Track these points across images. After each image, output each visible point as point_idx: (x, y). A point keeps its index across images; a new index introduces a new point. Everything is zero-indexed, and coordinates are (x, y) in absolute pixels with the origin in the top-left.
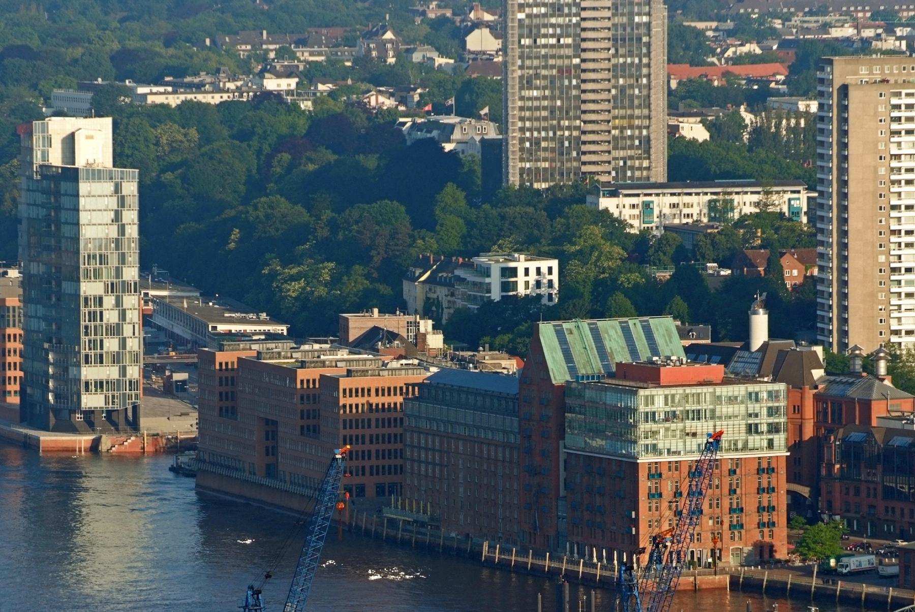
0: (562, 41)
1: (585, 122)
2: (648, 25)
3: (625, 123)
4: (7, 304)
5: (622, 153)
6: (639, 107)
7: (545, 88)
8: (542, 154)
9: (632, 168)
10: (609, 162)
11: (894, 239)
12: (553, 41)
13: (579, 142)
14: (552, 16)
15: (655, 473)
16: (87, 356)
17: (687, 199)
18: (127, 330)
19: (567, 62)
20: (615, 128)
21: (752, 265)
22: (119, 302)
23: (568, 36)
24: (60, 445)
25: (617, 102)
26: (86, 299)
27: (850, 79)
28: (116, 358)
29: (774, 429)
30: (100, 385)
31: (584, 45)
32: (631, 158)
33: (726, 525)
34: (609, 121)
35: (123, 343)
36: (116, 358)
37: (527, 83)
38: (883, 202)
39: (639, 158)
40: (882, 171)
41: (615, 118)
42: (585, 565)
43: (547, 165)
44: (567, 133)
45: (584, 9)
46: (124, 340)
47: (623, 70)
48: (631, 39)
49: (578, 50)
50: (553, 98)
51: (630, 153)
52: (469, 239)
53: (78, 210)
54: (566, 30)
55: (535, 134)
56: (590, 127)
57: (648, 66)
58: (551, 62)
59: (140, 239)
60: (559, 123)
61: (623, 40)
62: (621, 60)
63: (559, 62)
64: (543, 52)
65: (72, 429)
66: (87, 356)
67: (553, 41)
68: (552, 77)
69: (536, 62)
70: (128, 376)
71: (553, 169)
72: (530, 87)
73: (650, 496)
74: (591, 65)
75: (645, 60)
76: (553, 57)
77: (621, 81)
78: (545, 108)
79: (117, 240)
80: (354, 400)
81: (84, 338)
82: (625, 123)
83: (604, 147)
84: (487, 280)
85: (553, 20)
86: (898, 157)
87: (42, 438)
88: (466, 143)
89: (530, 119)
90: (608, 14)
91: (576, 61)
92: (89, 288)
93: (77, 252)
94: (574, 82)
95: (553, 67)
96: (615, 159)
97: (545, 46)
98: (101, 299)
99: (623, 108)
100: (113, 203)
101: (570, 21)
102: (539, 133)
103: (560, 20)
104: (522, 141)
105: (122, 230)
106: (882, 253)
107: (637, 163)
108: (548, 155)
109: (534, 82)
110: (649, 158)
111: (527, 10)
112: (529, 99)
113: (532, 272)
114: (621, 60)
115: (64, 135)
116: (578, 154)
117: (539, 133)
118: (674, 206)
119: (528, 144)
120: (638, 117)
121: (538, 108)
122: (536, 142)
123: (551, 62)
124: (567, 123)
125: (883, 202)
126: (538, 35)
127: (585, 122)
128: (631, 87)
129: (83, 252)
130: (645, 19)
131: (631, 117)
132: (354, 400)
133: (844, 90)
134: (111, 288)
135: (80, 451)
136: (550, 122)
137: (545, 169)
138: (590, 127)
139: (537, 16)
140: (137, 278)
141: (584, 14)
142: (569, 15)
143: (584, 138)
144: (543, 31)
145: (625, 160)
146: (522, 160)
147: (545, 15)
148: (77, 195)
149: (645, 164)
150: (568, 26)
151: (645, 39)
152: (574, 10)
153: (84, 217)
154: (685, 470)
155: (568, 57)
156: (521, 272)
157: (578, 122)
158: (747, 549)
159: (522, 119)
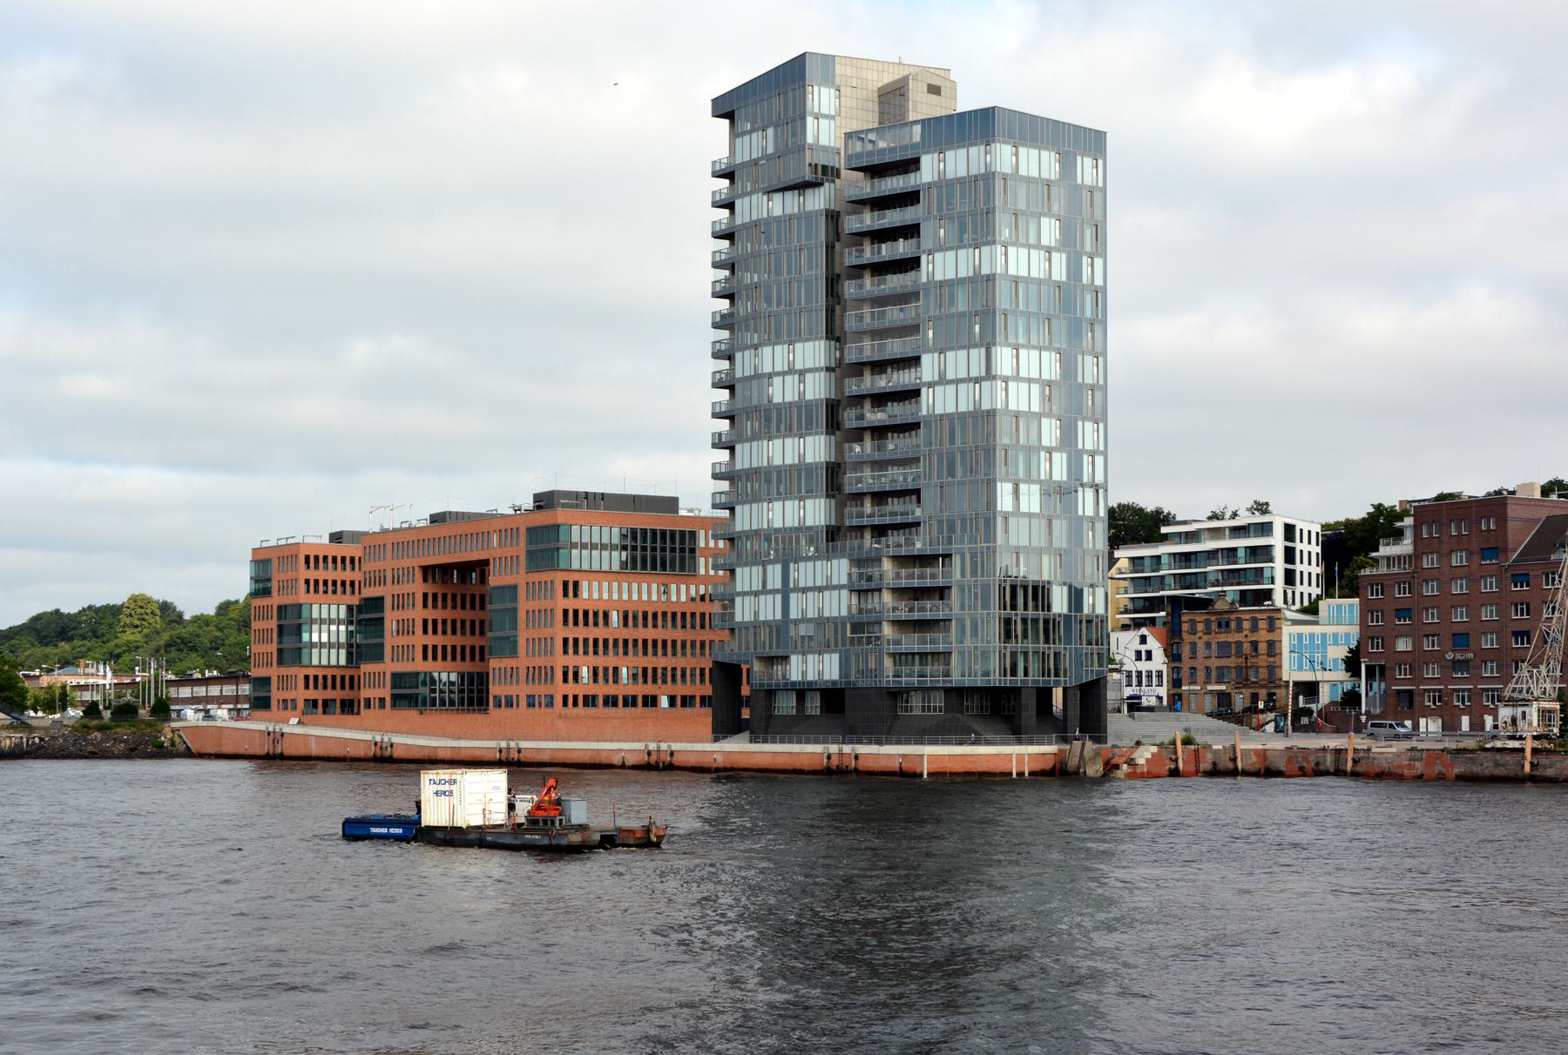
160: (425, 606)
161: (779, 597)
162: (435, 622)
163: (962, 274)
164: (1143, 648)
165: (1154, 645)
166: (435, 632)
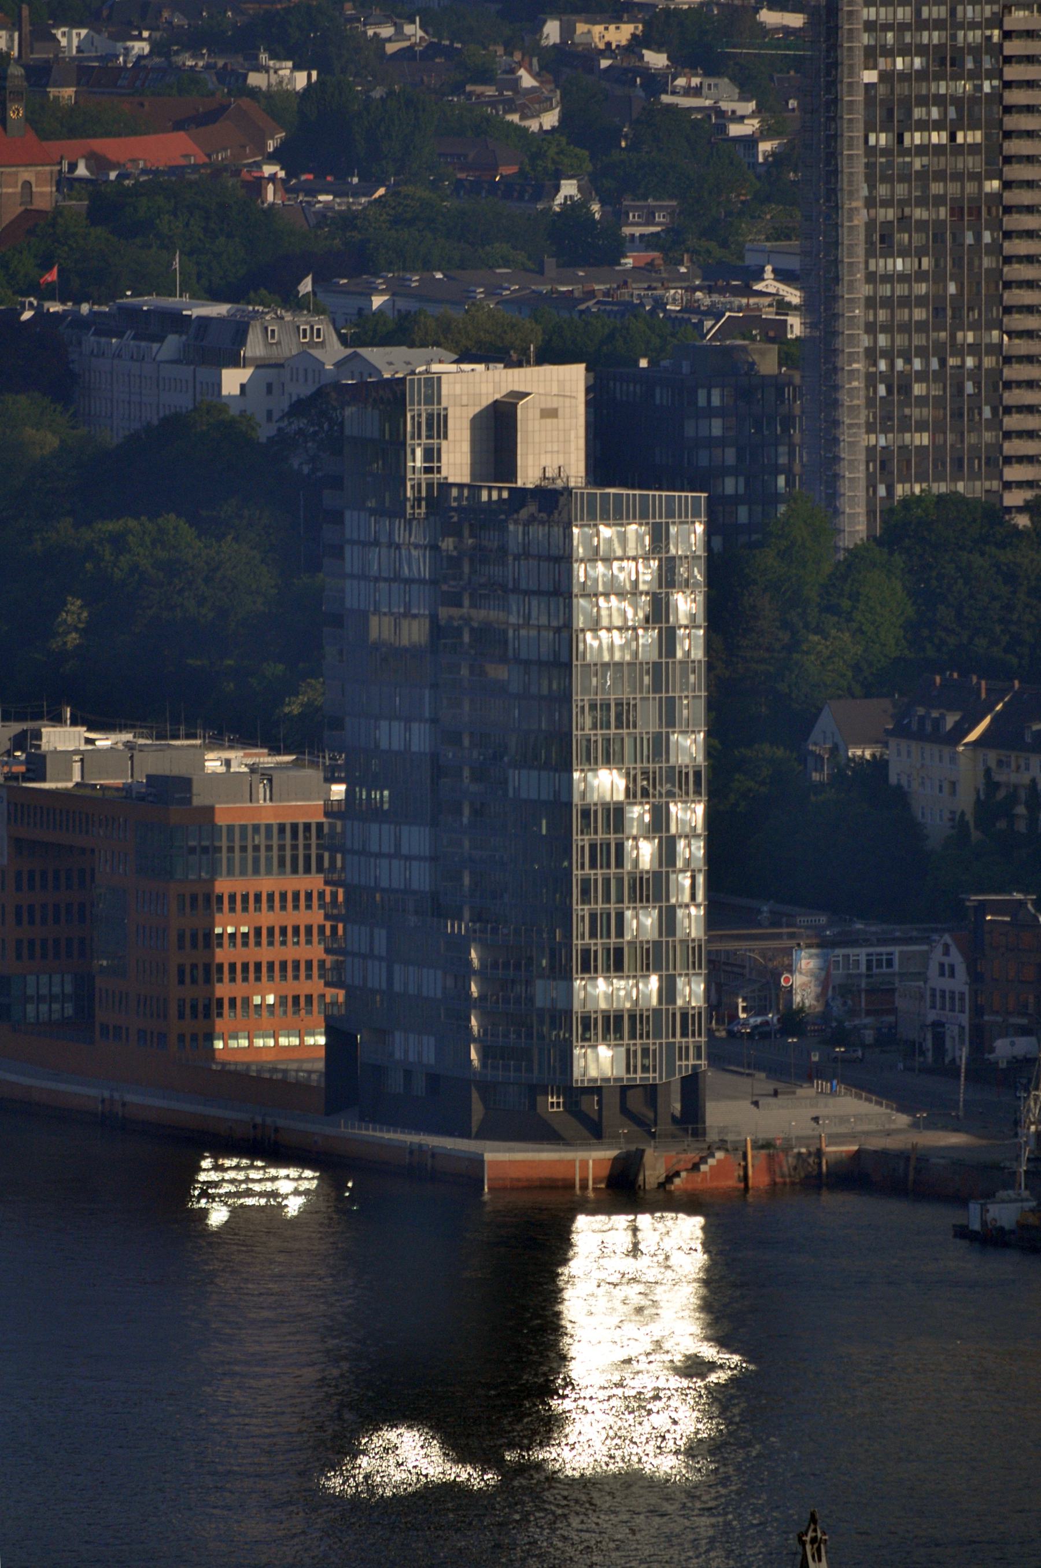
0: (960, 138)
14: (939, 77)
16: (586, 952)
19: (970, 187)
22: (659, 821)
23: (973, 127)
24: (514, 1173)
26: (586, 813)
31: (1013, 147)
35: (668, 920)
37: (882, 241)
43: (923, 439)
44: (970, 362)
45: (1008, 60)
46: (671, 911)
49: (997, 160)
50: (939, 277)
52: (925, 633)
53: (570, 596)
54: (967, 113)
55: (899, 364)
56: (1022, 346)
58: (936, 188)
59: (710, 666)
60: (953, 337)
63: (953, 189)
64: (917, 164)
65: (545, 1133)
68: (940, 224)
69: (901, 190)
71: (939, 449)
72: (888, 252)
74: (1025, 197)
76: (940, 176)
78: (921, 301)
79: (657, 666)
81: (580, 910)
87: (488, 1157)
88: (281, 366)
89: (887, 329)
93: (566, 698)
94: (987, 237)
95: (940, 200)
97: (922, 150)
101: (979, 88)
102: (908, 361)
103: (964, 87)
104: (871, 380)
105: (668, 640)
109: (897, 236)
111: (883, 63)
112: (888, 278)
115: (478, 409)
116: (994, 411)
117: (908, 361)
119: (882, 390)
121: (905, 302)
122: (901, 386)
123: (936, 188)
124: (970, 337)
127: (1010, 334)
135: (584, 1187)
136: (933, 335)
137: (921, 448)
138: (1022, 346)
139: (905, 76)
141: (1012, 73)
142: (975, 75)
143: (1010, 373)
146: (870, 429)
147: (922, 75)
150: (974, 100)
157: (995, 333)
159: (871, 328)
160: (19, 888)
161: (384, 964)
162: (31, 942)
163: (544, 797)
164: (946, 960)
165: (956, 958)
166: (32, 922)
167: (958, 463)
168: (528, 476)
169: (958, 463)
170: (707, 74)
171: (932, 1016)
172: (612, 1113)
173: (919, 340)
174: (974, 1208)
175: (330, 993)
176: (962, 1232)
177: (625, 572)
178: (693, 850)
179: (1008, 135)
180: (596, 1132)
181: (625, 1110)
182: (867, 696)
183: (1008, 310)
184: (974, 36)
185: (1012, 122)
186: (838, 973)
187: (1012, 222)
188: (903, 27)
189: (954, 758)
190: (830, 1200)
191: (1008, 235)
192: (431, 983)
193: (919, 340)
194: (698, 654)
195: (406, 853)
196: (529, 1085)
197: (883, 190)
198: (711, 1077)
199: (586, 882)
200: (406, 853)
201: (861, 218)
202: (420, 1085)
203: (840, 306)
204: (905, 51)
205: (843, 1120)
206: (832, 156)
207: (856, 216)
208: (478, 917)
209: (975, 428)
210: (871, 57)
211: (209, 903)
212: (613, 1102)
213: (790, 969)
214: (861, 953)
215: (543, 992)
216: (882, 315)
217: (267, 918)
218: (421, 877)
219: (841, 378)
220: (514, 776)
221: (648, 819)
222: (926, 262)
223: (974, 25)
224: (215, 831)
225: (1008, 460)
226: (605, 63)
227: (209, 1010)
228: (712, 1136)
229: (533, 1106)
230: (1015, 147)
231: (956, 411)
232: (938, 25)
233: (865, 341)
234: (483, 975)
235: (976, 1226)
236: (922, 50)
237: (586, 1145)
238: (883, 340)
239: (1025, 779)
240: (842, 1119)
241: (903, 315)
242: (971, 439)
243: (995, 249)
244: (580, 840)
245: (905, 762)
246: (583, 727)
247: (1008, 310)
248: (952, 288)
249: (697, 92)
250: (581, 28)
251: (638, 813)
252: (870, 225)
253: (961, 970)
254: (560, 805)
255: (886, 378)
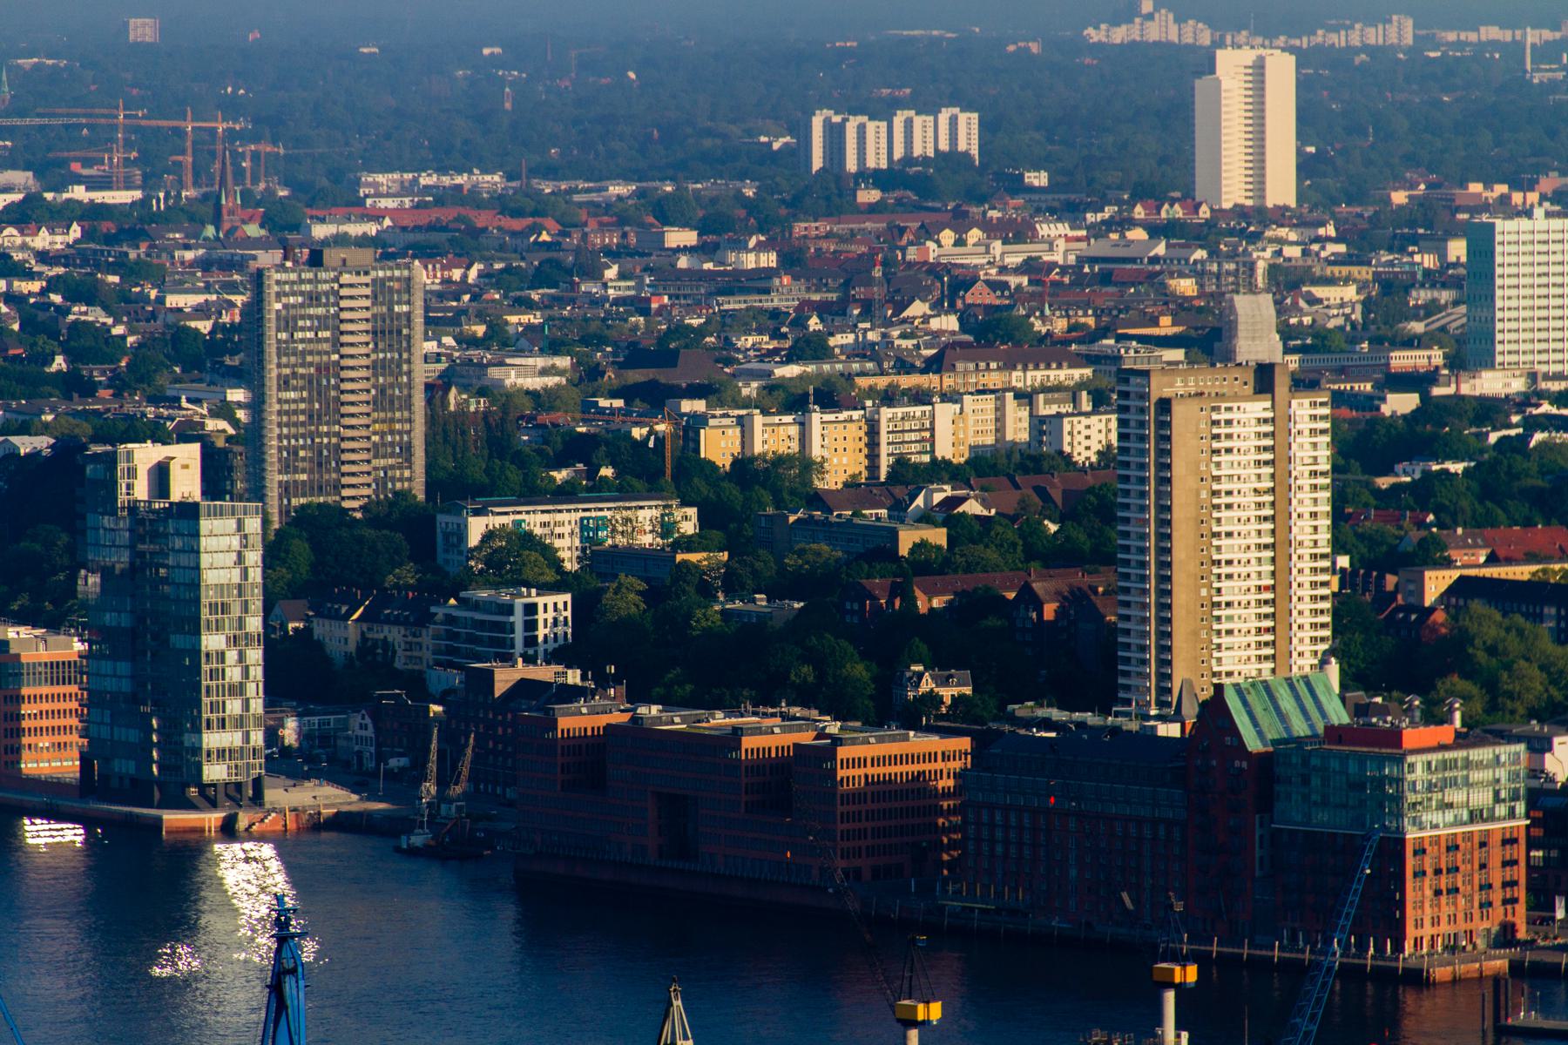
1: (345, 427)
2: (408, 315)
3: (385, 427)
4: (23, 660)
5: (382, 462)
6: (400, 409)
7: (302, 389)
8: (300, 465)
9: (393, 479)
10: (369, 473)
11: (1216, 570)
12: (310, 335)
13: (339, 450)
14: (310, 306)
15: (1420, 852)
16: (208, 721)
17: (559, 517)
18: (251, 689)
19: (325, 358)
20: (375, 433)
21: (875, 598)
22: (241, 657)
23: (327, 329)
24: (181, 824)
25: (376, 404)
26: (207, 655)
27: (1167, 392)
28: (240, 722)
29: (1515, 797)
30: (221, 753)
32: (392, 467)
33: (1476, 904)
34: (368, 426)
35: (246, 705)
36: (240, 722)
37: (285, 384)
38: (1204, 528)
39: (400, 468)
40: (1204, 495)
41: (375, 422)
42: (1312, 952)
43: (304, 477)
44: (325, 440)
47: (383, 367)
48: (391, 332)
49: (337, 345)
51: (391, 461)
53: (198, 552)
54: (323, 322)
55: (293, 442)
56: (349, 433)
57: (409, 362)
58: (309, 359)
59: (265, 585)
61: (383, 332)
62: (381, 355)
63: (317, 359)
64: (300, 347)
65: (189, 806)
66: (208, 721)
67: (310, 335)
68: (310, 375)
69: (293, 359)
70: (252, 743)
71: (311, 481)
73: (1415, 875)
74: (350, 362)
75: (405, 356)
76: (311, 353)
77: (381, 380)
78: (303, 412)
80: (851, 772)
81: (205, 700)
82: (385, 427)
83: (364, 456)
84: (512, 619)
85: (312, 311)
86: (1217, 479)
87: (165, 817)
89: (287, 425)
90: (368, 303)
91: (335, 357)
92: (212, 641)
93: (197, 601)
94: (333, 381)
95: (311, 364)
96: (376, 469)
97: (302, 341)
98: (223, 653)
99: (383, 410)
100: (235, 542)
103: (320, 311)
104: (280, 449)
105: (245, 574)
106: (1204, 586)
107: (398, 473)
108: (306, 465)
110: (410, 467)
111: (284, 300)
112: (287, 401)
113: (550, 608)
114: (381, 355)
118: (544, 525)
120: (399, 421)
123: (309, 359)
124: (325, 429)
125: (1204, 528)
126: (296, 328)
128: (392, 386)
129: (204, 601)
130: (405, 308)
131: (392, 420)
132: (851, 772)
133: (1165, 405)
134: (234, 641)
138: (349, 433)
139: (294, 306)
140: (261, 630)
141: (343, 304)
142: (326, 305)
143: (344, 445)
144: (300, 323)
145: (385, 469)
146: (280, 472)
147: (302, 305)
148: (198, 535)
149: (407, 473)
150: (326, 317)
151: (405, 331)
152: (332, 300)
153: (205, 560)
154: (1443, 844)
155: (327, 353)
156: (541, 608)
158: (1495, 929)
159: (280, 425)
165: (368, 720)
167: (320, 488)
168: (175, 496)
169: (320, 488)
170: (87, 305)
171: (357, 748)
172: (221, 796)
173: (302, 430)
174: (404, 838)
175: (81, 741)
176: (398, 850)
177: (224, 542)
178: (257, 673)
179: (342, 333)
180: (213, 804)
181: (227, 795)
182: (295, 598)
183: (343, 416)
184: (326, 287)
185: (344, 327)
186: (305, 729)
187: (344, 374)
188: (293, 283)
189: (346, 627)
190: (325, 835)
191: (342, 380)
192: (133, 735)
193: (302, 430)
194: (259, 579)
195: (119, 676)
196: (182, 783)
197: (284, 360)
198: (267, 781)
199: (208, 687)
200: (119, 676)
201: (274, 374)
202: (127, 782)
203: (265, 415)
204: (294, 294)
205: (327, 797)
206: (261, 344)
207: (272, 372)
208: (155, 704)
209: (328, 471)
210: (279, 295)
211: (19, 699)
212: (221, 790)
213: (283, 726)
214: (315, 719)
215: (188, 740)
216: (285, 419)
217: (45, 706)
218: (126, 686)
219: (266, 449)
220: (173, 638)
221: (233, 657)
222: (305, 394)
223: (326, 282)
224: (20, 665)
225: (343, 487)
226: (32, 300)
227: (16, 751)
228: (268, 806)
229: (183, 792)
230: (345, 339)
231: (319, 464)
232: (310, 281)
233: (277, 431)
234: (158, 731)
235: (405, 846)
236: (302, 293)
237: (209, 811)
238: (285, 431)
239: (381, 636)
240: (327, 797)
241: (294, 418)
242: (326, 477)
243: (337, 387)
244: (205, 667)
245: (321, 629)
246: (205, 614)
247: (343, 416)
248: (317, 406)
249: (86, 313)
250: (16, 284)
251: (231, 656)
252: (279, 376)
253: (370, 726)
254: (195, 652)
255: (287, 449)
